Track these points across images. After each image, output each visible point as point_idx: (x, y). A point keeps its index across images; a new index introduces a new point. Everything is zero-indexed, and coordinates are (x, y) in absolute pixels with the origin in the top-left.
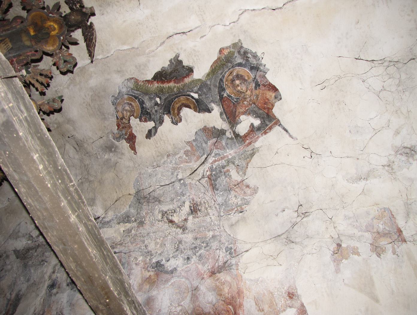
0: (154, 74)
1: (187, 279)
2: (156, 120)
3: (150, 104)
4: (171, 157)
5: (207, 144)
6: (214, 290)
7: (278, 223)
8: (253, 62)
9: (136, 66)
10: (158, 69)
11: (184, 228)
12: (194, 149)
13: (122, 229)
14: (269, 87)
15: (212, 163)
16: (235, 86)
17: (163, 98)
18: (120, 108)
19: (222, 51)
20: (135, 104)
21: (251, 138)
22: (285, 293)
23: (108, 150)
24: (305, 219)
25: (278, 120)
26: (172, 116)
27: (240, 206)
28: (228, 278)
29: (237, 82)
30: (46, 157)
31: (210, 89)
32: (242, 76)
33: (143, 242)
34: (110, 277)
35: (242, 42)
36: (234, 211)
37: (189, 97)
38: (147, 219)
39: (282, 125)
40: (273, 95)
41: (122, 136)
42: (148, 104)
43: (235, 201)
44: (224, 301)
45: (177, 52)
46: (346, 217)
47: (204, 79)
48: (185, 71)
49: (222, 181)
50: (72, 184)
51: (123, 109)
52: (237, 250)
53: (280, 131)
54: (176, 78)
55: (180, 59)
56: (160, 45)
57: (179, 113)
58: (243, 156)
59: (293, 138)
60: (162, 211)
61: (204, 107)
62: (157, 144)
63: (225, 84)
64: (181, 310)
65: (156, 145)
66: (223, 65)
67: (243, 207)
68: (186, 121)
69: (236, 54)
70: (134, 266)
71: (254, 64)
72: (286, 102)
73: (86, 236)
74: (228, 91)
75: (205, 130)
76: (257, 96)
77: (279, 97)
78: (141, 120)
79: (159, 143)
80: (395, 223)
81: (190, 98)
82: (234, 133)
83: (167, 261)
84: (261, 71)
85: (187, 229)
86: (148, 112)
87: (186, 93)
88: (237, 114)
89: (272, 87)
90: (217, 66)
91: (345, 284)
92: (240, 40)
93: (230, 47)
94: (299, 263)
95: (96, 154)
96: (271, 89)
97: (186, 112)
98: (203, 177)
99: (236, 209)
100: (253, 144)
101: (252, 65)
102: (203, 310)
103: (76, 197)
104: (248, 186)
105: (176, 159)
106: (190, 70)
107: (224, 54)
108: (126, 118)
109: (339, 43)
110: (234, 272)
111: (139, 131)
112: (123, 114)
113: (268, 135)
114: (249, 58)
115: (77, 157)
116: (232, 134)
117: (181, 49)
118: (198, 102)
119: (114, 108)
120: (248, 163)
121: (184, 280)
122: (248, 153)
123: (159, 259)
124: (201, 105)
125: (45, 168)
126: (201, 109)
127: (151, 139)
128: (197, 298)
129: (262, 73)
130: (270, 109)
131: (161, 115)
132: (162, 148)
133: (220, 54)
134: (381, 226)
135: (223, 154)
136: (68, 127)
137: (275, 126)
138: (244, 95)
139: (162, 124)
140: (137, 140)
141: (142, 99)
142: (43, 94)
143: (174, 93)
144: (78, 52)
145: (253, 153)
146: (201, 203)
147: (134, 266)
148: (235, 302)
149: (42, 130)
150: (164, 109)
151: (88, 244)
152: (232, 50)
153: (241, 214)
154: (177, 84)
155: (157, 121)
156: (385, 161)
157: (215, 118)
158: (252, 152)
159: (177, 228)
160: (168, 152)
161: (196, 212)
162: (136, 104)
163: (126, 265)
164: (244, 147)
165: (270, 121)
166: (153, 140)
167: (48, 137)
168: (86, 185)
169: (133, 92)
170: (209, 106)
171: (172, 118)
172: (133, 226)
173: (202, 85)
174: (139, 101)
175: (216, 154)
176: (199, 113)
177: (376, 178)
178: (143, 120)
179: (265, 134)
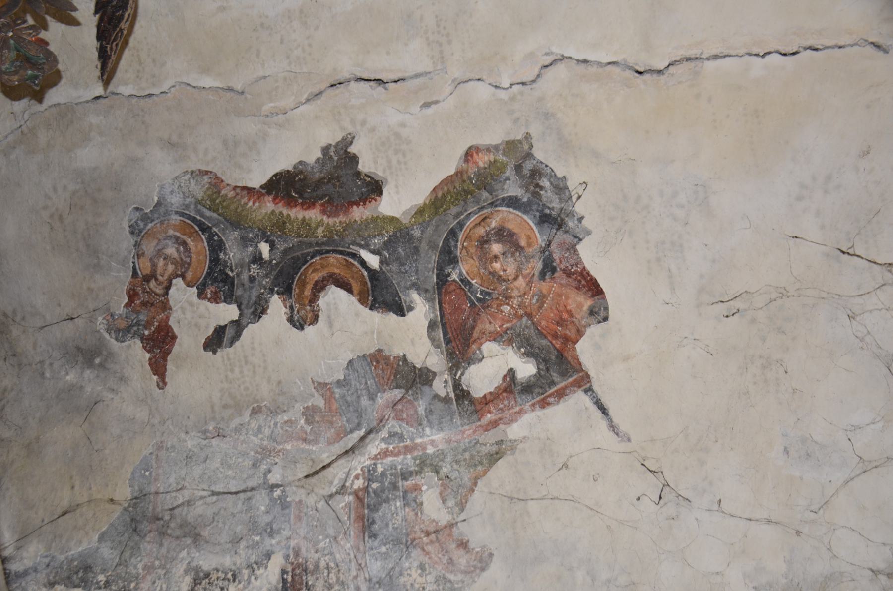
3: (238, 256)
4: (261, 418)
8: (551, 202)
9: (225, 142)
12: (334, 407)
14: (580, 281)
15: (376, 456)
16: (486, 258)
17: (281, 247)
18: (149, 247)
19: (472, 156)
20: (196, 247)
21: (501, 409)
29: (496, 248)
31: (416, 250)
32: (511, 234)
39: (593, 392)
40: (588, 304)
41: (135, 328)
42: (233, 254)
45: (350, 129)
47: (405, 221)
48: (358, 187)
51: (159, 253)
55: (352, 149)
57: (314, 298)
58: (467, 455)
59: (617, 434)
61: (389, 299)
62: (232, 371)
65: (229, 373)
66: (468, 192)
68: (331, 324)
69: (509, 172)
75: (377, 358)
76: (542, 298)
78: (201, 295)
79: (237, 370)
81: (356, 263)
84: (566, 232)
86: (227, 275)
87: (349, 248)
88: (476, 334)
89: (587, 282)
90: (449, 192)
93: (496, 147)
96: (584, 286)
101: (547, 211)
105: (276, 424)
106: (375, 188)
107: (476, 163)
108: (160, 278)
112: (154, 266)
113: (549, 410)
114: (542, 188)
116: (450, 389)
118: (377, 280)
119: (133, 242)
122: (485, 450)
127: (220, 353)
129: (568, 238)
131: (263, 294)
132: (242, 387)
133: (466, 161)
135: (412, 439)
137: (575, 392)
138: (507, 289)
139: (260, 317)
140: (176, 349)
141: (219, 236)
145: (497, 453)
152: (500, 157)
154: (329, 216)
155: (247, 308)
157: (412, 334)
158: (494, 448)
160: (257, 401)
162: (199, 247)
164: (475, 432)
165: (564, 374)
166: (223, 357)
170: (403, 297)
171: (291, 308)
173: (398, 238)
174: (210, 239)
176: (371, 309)
178: (209, 296)
179: (543, 407)
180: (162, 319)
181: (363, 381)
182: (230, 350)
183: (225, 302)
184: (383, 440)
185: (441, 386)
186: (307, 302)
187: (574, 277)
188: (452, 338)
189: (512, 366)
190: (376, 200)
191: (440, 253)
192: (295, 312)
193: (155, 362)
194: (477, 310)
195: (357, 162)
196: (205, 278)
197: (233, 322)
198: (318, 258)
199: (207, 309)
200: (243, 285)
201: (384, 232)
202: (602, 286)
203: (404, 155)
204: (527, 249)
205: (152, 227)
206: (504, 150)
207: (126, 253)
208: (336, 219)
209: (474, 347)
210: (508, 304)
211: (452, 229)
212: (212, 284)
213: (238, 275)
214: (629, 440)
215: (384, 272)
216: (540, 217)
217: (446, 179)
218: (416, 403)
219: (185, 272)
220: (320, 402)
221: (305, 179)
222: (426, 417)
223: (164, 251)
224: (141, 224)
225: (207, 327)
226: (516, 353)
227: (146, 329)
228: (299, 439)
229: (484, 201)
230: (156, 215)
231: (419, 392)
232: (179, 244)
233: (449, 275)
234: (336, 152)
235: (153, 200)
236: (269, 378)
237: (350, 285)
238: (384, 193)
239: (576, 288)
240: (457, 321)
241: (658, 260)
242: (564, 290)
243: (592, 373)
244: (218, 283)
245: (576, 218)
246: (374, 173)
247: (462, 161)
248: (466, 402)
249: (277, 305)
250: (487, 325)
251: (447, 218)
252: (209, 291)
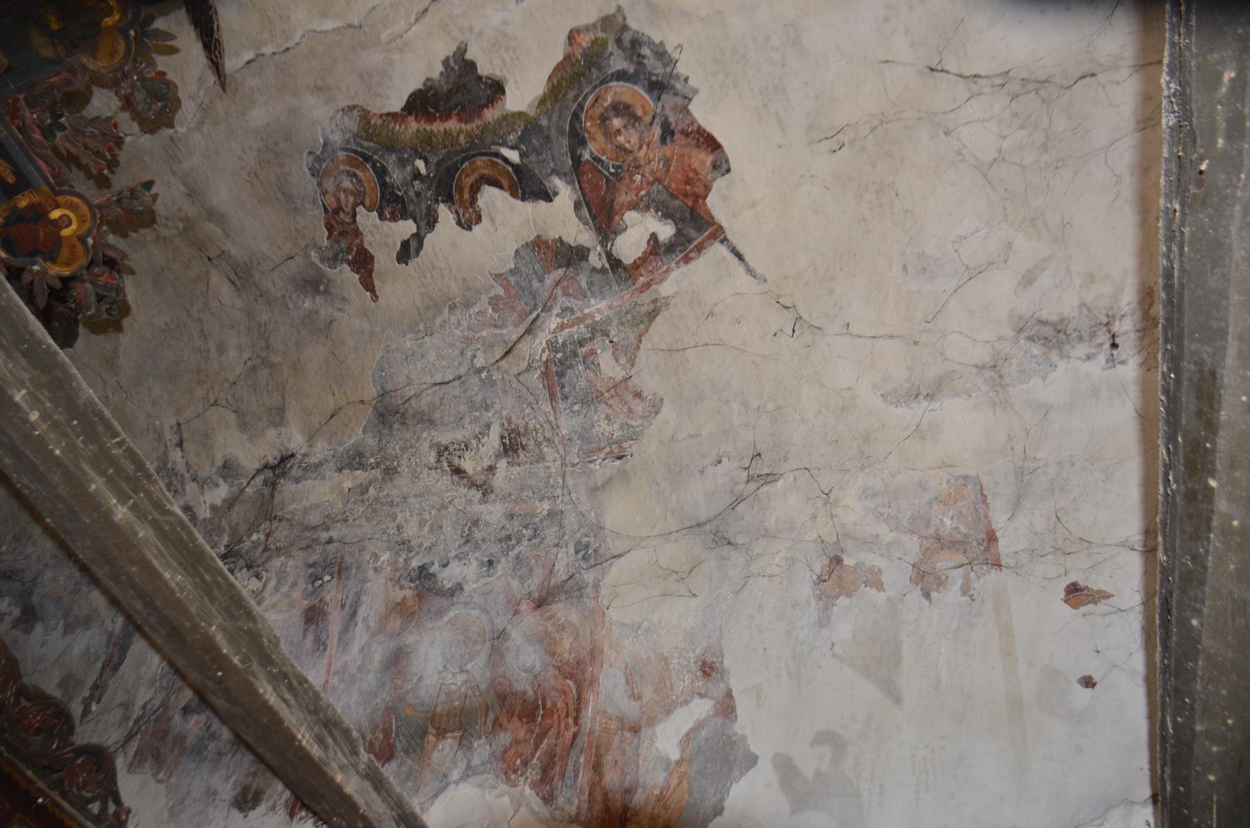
1: (485, 611)
3: (401, 176)
4: (458, 313)
6: (541, 642)
7: (701, 496)
9: (361, 76)
10: (415, 84)
11: (485, 490)
13: (348, 484)
16: (610, 135)
17: (434, 160)
18: (329, 185)
22: (696, 662)
23: (309, 289)
24: (764, 489)
25: (720, 229)
26: (457, 206)
27: (619, 442)
28: (574, 617)
29: (617, 123)
30: (46, 392)
31: (548, 138)
32: (627, 107)
33: (394, 517)
34: (222, 628)
35: (626, 13)
36: (602, 455)
38: (404, 462)
42: (396, 176)
43: (608, 429)
44: (559, 668)
45: (461, 38)
46: (867, 493)
47: (532, 113)
49: (579, 377)
50: (118, 439)
51: (338, 188)
52: (601, 551)
54: (463, 109)
55: (468, 56)
56: (417, 20)
57: (473, 200)
60: (438, 445)
62: (425, 277)
64: (465, 682)
66: (580, 75)
67: (624, 445)
68: (493, 221)
69: (612, 47)
70: (371, 573)
71: (658, 75)
73: (156, 547)
76: (667, 162)
77: (725, 167)
78: (381, 217)
79: (428, 276)
80: (986, 516)
82: (609, 256)
83: (444, 566)
84: (676, 94)
85: (492, 492)
88: (616, 208)
90: (563, 78)
91: (834, 655)
92: (619, 9)
93: (594, 26)
94: (737, 593)
95: (283, 297)
97: (492, 198)
98: (529, 368)
99: (608, 449)
100: (654, 287)
101: (654, 78)
102: (511, 685)
103: (130, 467)
104: (638, 395)
106: (497, 89)
107: (580, 45)
109: (887, 20)
110: (590, 603)
112: (338, 200)
113: (692, 265)
114: (644, 57)
115: (239, 303)
116: (605, 260)
117: (471, 29)
120: (640, 336)
121: (476, 612)
122: (643, 310)
123: (426, 561)
125: (45, 416)
126: (528, 190)
128: (502, 656)
130: (699, 197)
133: (571, 44)
134: (948, 522)
135: (581, 311)
136: (210, 228)
140: (376, 266)
142: (103, 183)
144: (185, 63)
146: (526, 429)
147: (371, 573)
148: (583, 673)
149: (32, 334)
150: (437, 188)
151: (161, 563)
152: (600, 34)
153: (618, 463)
156: (982, 354)
157: (561, 216)
158: (651, 307)
159: (469, 488)
161: (516, 451)
162: (367, 175)
163: (354, 571)
165: (700, 230)
167: (49, 346)
168: (264, 372)
169: (358, 144)
171: (457, 212)
172: (371, 476)
173: (529, 130)
174: (374, 167)
175: (564, 310)
176: (523, 200)
177: (957, 395)
182: (418, 259)
184: (557, 315)
199: (390, 228)
209: (617, 218)
213: (406, 193)
221: (436, 93)
224: (317, 165)
234: (455, 62)
241: (765, 106)
243: (724, 224)
244: (393, 204)
249: (445, 214)
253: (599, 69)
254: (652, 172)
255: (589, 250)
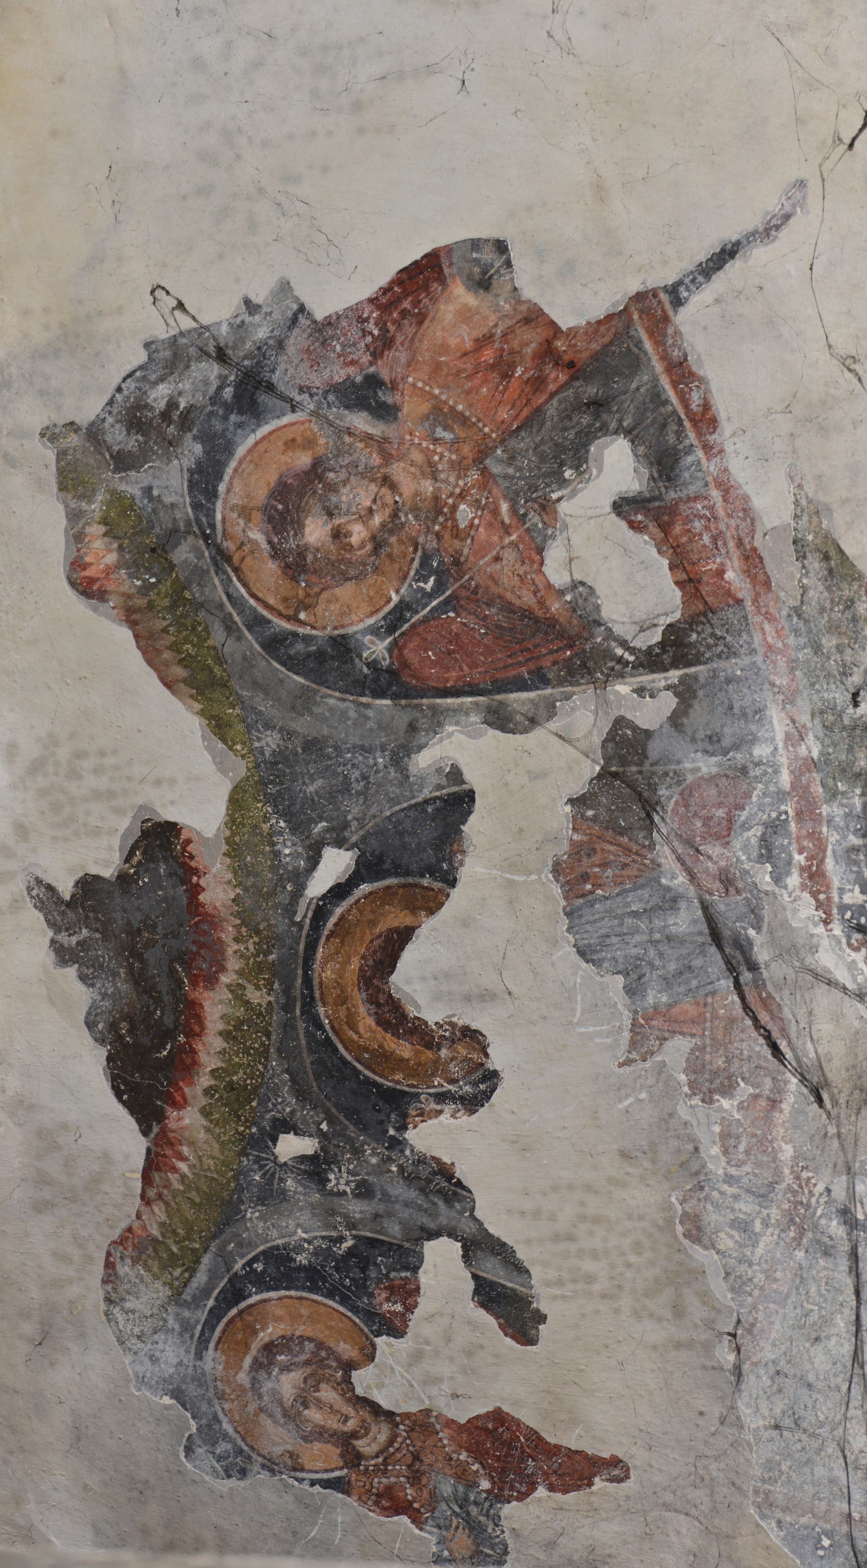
0: (120, 1107)
2: (426, 1221)
3: (305, 1217)
4: (712, 1218)
5: (674, 900)
8: (206, 382)
9: (40, 1207)
10: (90, 1064)
12: (693, 1011)
14: (404, 313)
15: (819, 906)
16: (340, 566)
17: (287, 1103)
18: (278, 1438)
19: (92, 581)
20: (278, 1319)
21: (715, 539)
29: (315, 531)
31: (313, 745)
32: (281, 490)
37: (332, 920)
39: (680, 283)
40: (460, 294)
41: (474, 1510)
42: (298, 1228)
45: (19, 885)
47: (241, 768)
48: (156, 883)
51: (292, 1416)
53: (717, 301)
55: (66, 888)
57: (419, 1033)
58: (829, 642)
59: (787, 217)
61: (428, 832)
62: (590, 1279)
63: (307, 630)
65: (597, 1287)
66: (178, 598)
68: (486, 996)
69: (131, 485)
72: (529, 209)
74: (360, 624)
75: (576, 877)
76: (441, 415)
77: (488, 255)
78: (395, 1328)
79: (589, 1266)
81: (339, 911)
84: (281, 345)
86: (350, 1252)
87: (300, 925)
88: (527, 599)
89: (406, 294)
90: (175, 647)
92: (49, 434)
93: (74, 516)
96: (416, 303)
101: (228, 393)
105: (729, 1179)
106: (159, 840)
107: (108, 571)
108: (351, 1425)
111: (464, 1371)
112: (321, 1434)
113: (722, 407)
114: (172, 404)
116: (659, 680)
118: (380, 859)
119: (264, 1475)
122: (817, 592)
124: (404, 846)
127: (543, 1305)
129: (297, 341)
131: (401, 1169)
132: (633, 1258)
133: (101, 596)
135: (781, 796)
137: (677, 333)
138: (415, 509)
139: (459, 1184)
140: (528, 1417)
141: (255, 1259)
143: (276, 1018)
145: (826, 557)
152: (96, 507)
154: (223, 969)
155: (434, 1215)
157: (520, 774)
158: (814, 563)
160: (670, 1222)
162: (281, 1313)
164: (769, 617)
165: (634, 362)
166: (554, 1298)
170: (426, 793)
171: (442, 1098)
173: (279, 793)
174: (262, 1282)
176: (453, 883)
178: (399, 1308)
179: (713, 423)
180: (452, 1438)
181: (629, 921)
182: (537, 1273)
183: (415, 1269)
184: (778, 879)
185: (648, 704)
186: (429, 1054)
187: (392, 328)
188: (532, 666)
189: (608, 509)
190: (189, 841)
191: (323, 683)
192: (452, 1088)
193: (560, 1476)
194: (464, 593)
195: (97, 878)
196: (355, 1310)
197: (467, 1258)
198: (321, 1010)
199: (430, 1318)
200: (377, 1216)
201: (265, 827)
202: (418, 256)
203: (80, 755)
204: (320, 451)
205: (231, 1421)
206: (82, 497)
207: (289, 1498)
208: (230, 951)
209: (555, 607)
210: (454, 508)
211: (264, 646)
212: (371, 1295)
213: (352, 1225)
214: (801, 184)
215: (364, 838)
216: (240, 412)
217: (145, 654)
218: (690, 778)
219: (338, 1359)
220: (678, 1049)
221: (129, 1018)
222: (725, 753)
223: (288, 1403)
224: (223, 1447)
225: (474, 1326)
226: (574, 493)
227: (476, 1485)
228: (767, 1119)
229: (200, 556)
230: (204, 1407)
231: (660, 769)
232: (271, 1363)
233: (373, 665)
234: (70, 930)
235: (167, 1408)
236: (611, 1180)
237: (390, 930)
238: (171, 818)
239: (420, 323)
240: (489, 651)
241: (357, 107)
242: (425, 356)
243: (634, 286)
244: (368, 1280)
245: (248, 319)
246: (124, 837)
247: (102, 607)
248: (694, 636)
249: (435, 1135)
250: (505, 572)
251: (238, 657)
252: (385, 1307)
253: (173, 536)
254: (460, 468)
255: (620, 722)
